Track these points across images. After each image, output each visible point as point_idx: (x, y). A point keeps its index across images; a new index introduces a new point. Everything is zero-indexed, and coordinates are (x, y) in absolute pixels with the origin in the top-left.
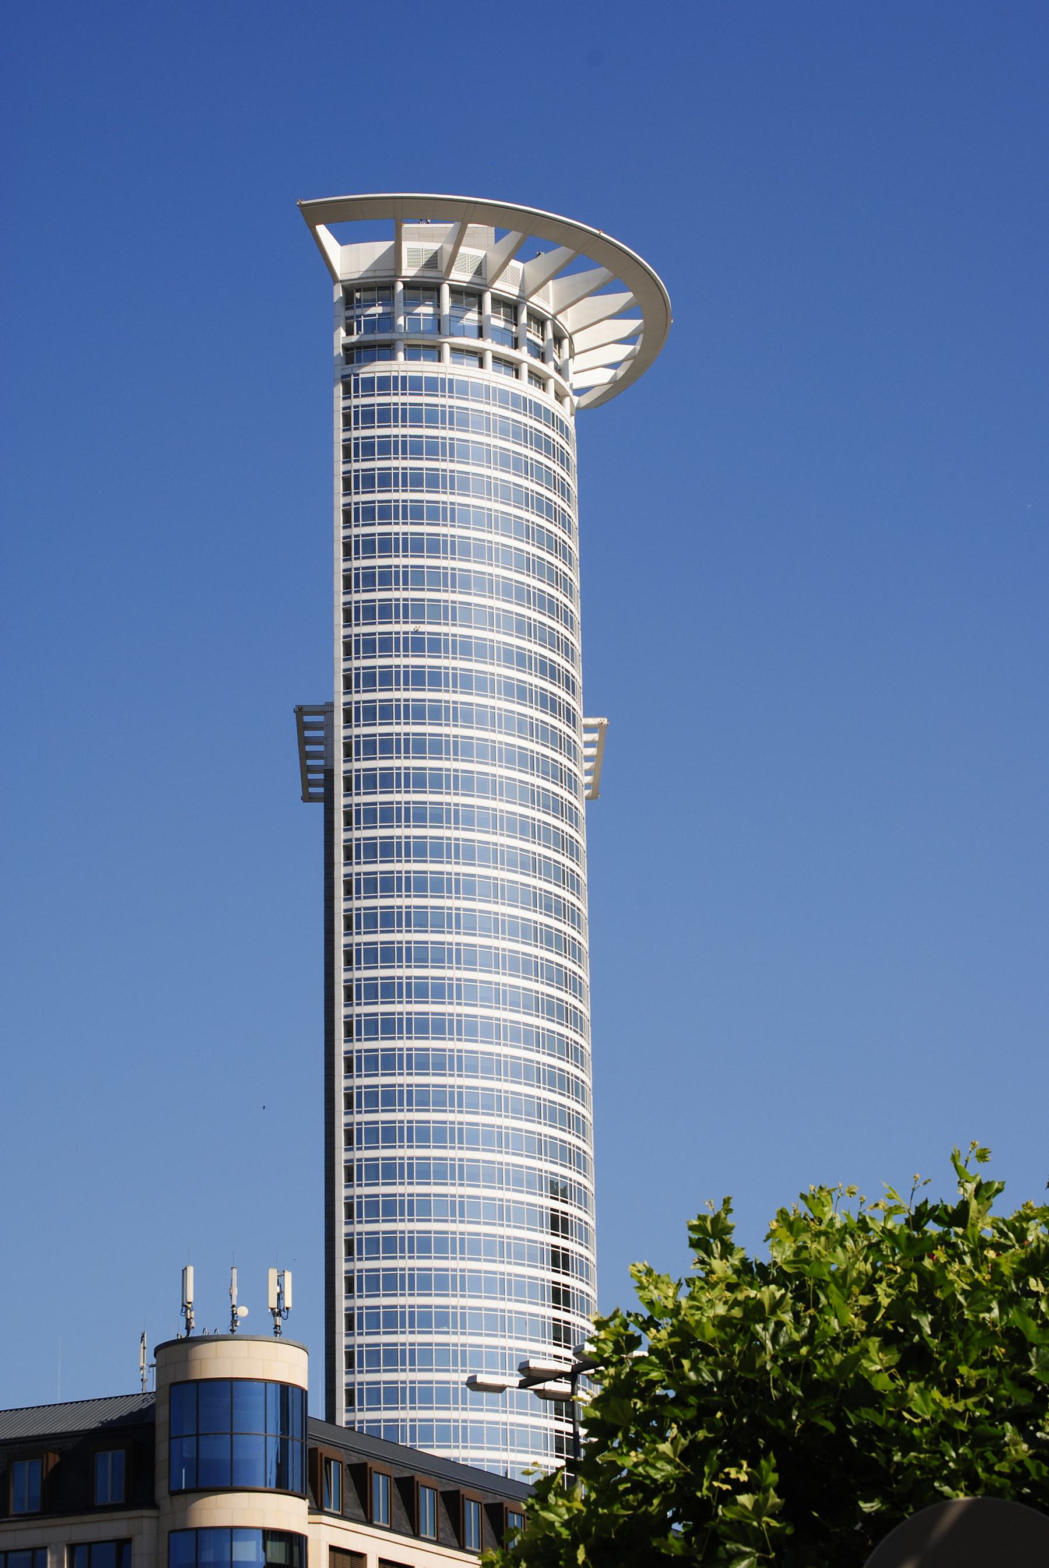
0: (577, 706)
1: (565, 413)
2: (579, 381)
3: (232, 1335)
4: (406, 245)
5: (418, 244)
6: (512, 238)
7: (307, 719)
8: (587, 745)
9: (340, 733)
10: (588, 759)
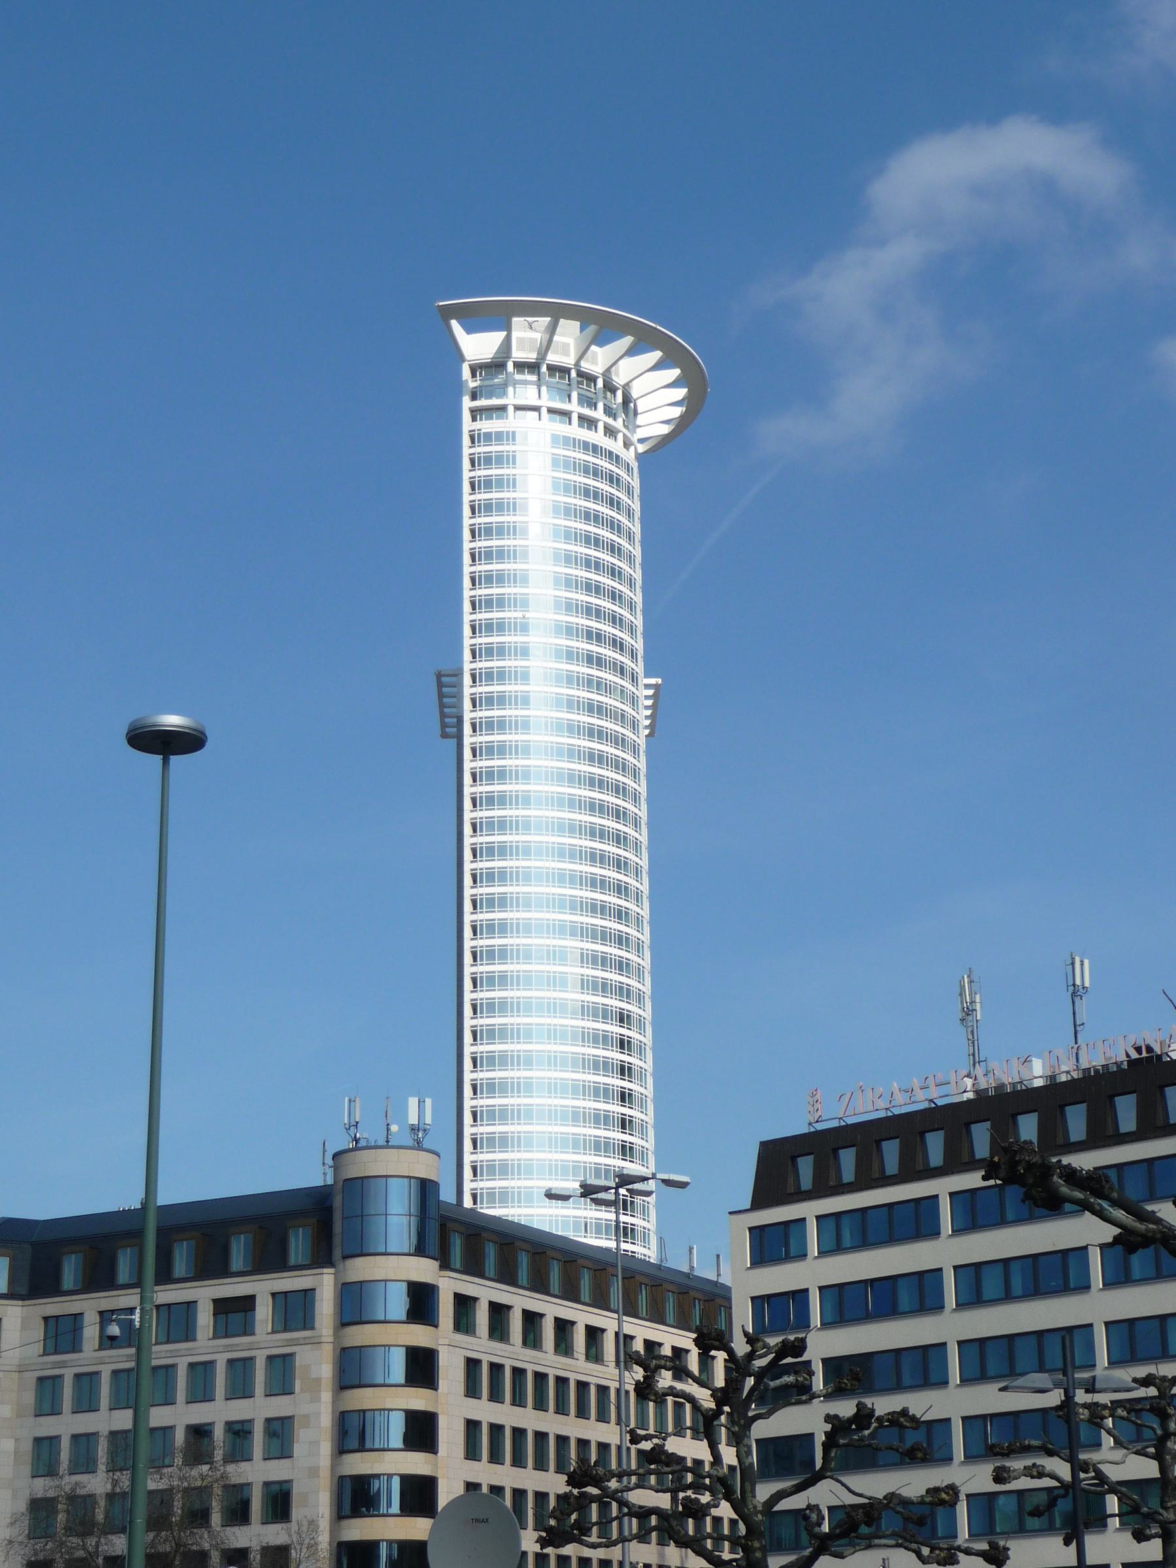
0: (640, 669)
1: (629, 456)
2: (641, 433)
3: (387, 1146)
4: (515, 335)
5: (526, 335)
6: (592, 329)
7: (444, 679)
8: (647, 697)
9: (467, 691)
10: (647, 708)
